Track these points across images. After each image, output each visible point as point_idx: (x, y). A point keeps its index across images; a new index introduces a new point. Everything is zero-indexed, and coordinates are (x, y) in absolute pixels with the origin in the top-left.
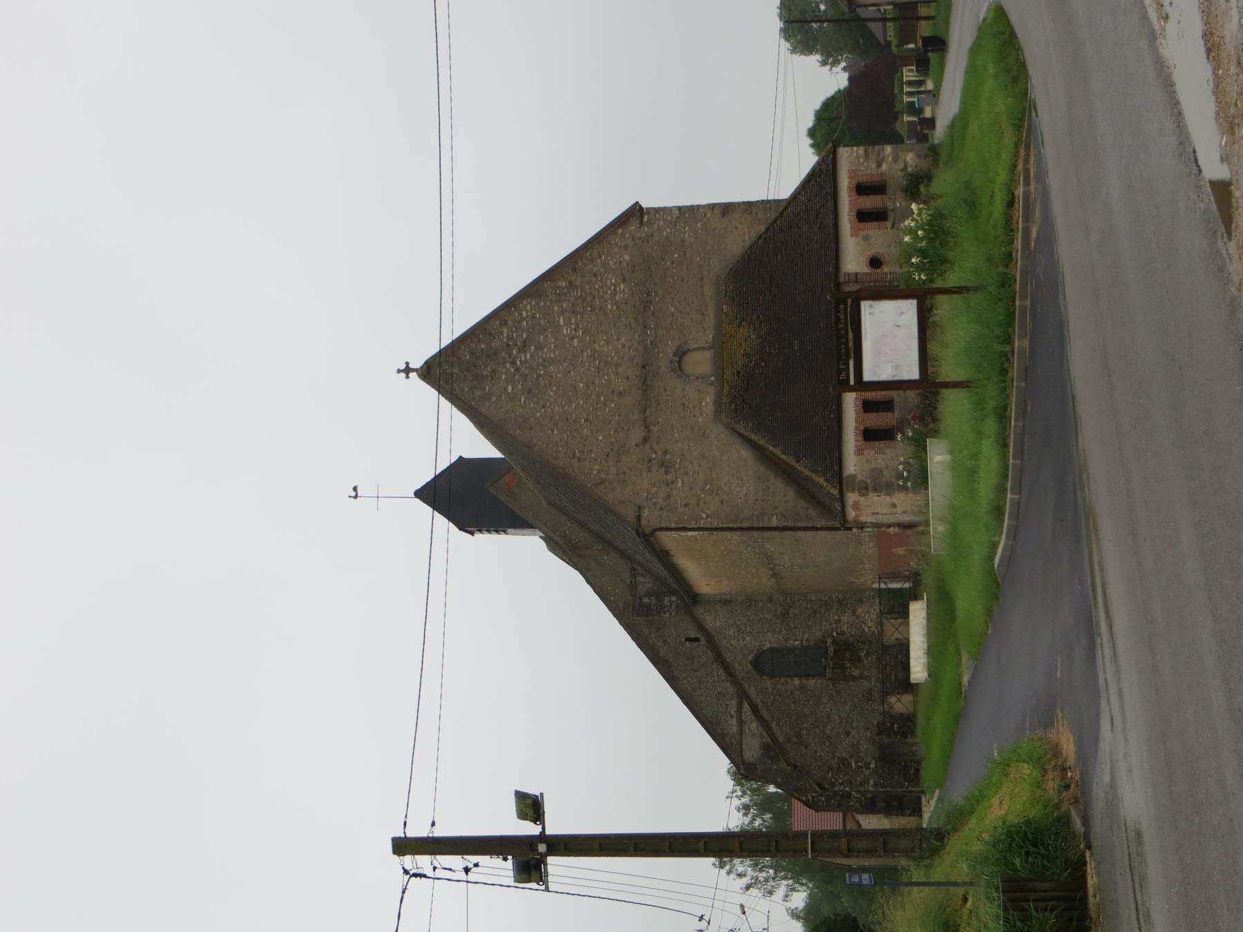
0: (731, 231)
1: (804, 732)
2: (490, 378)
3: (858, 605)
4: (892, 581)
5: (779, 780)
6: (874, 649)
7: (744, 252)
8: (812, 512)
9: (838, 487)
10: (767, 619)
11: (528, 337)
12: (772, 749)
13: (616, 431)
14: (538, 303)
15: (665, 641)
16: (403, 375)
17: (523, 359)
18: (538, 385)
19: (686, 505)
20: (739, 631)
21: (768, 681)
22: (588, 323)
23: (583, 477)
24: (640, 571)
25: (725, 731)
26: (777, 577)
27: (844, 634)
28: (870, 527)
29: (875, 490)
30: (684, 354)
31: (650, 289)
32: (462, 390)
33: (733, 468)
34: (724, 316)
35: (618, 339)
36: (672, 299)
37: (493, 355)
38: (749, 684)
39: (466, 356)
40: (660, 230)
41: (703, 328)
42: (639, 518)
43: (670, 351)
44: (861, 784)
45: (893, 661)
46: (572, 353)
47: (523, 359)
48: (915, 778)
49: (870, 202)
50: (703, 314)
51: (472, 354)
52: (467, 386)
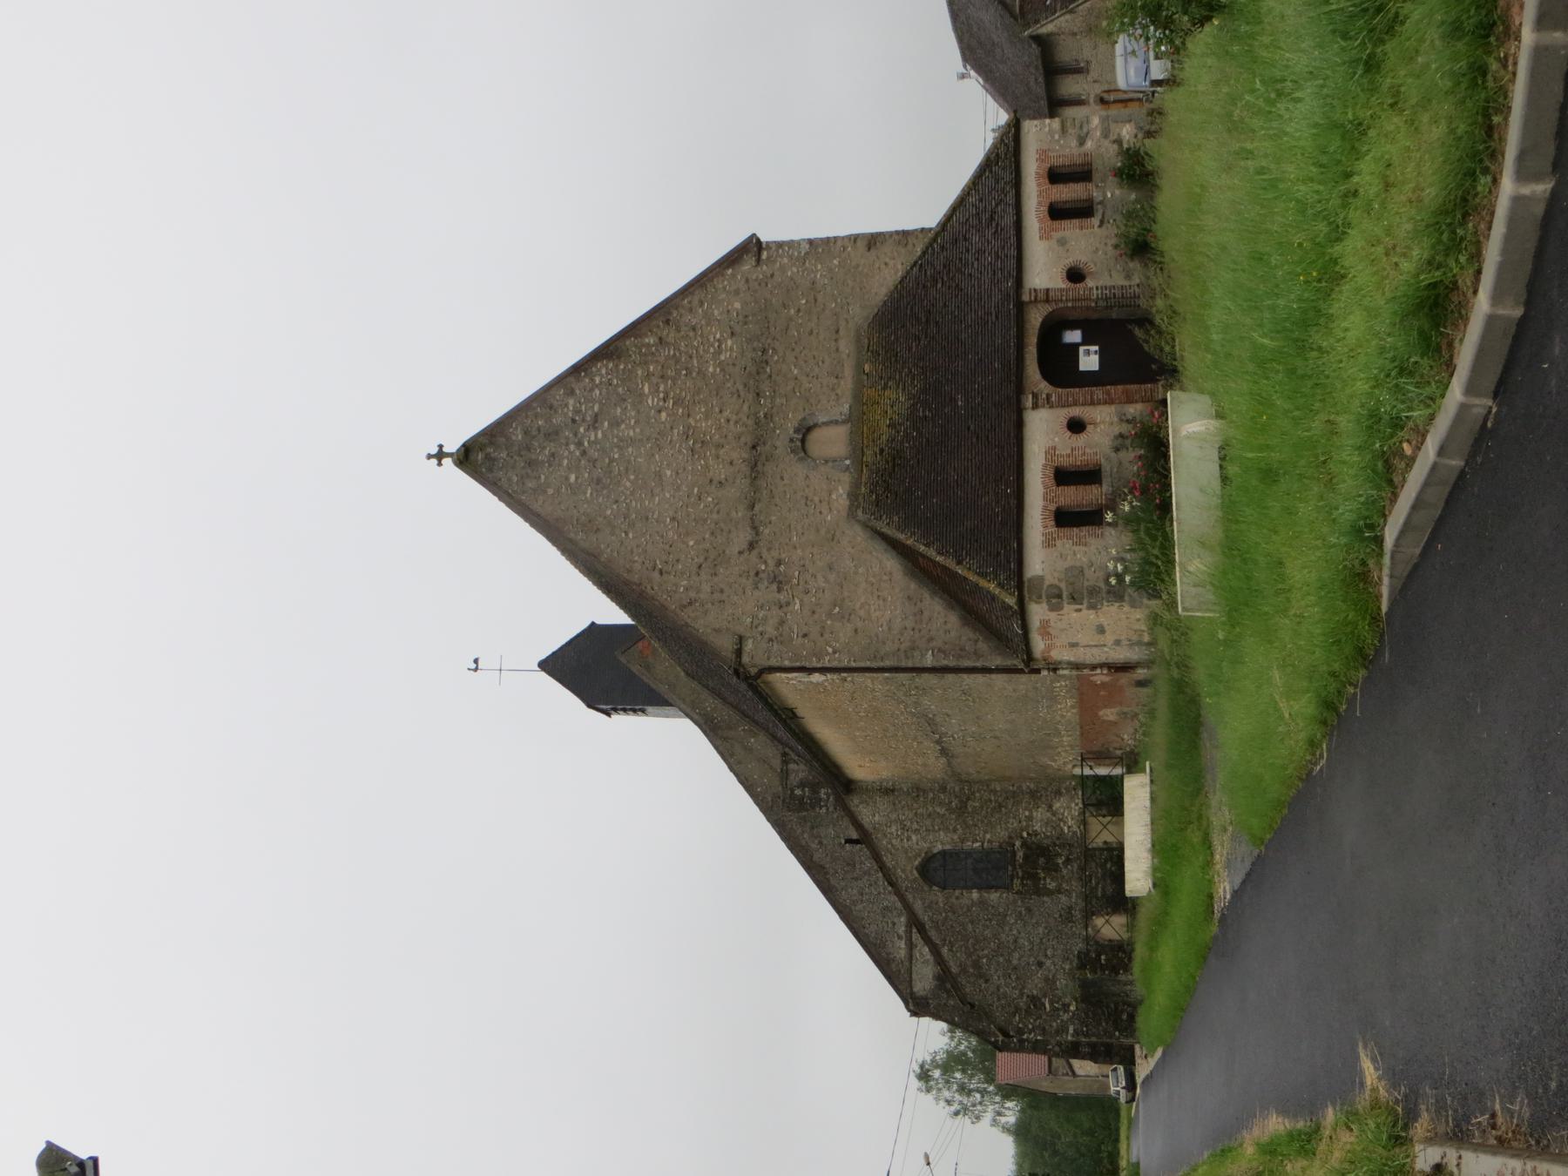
0: (879, 268)
1: (984, 960)
2: (547, 465)
3: (1055, 797)
4: (1100, 765)
5: (956, 1019)
6: (1075, 855)
7: (892, 288)
8: (983, 646)
9: (1016, 593)
10: (938, 813)
11: (601, 409)
12: (945, 977)
13: (712, 533)
14: (617, 366)
15: (820, 843)
16: (434, 461)
17: (593, 438)
18: (611, 472)
19: (805, 635)
20: (903, 829)
21: (939, 894)
22: (681, 390)
23: (665, 597)
24: (793, 755)
25: (892, 956)
26: (947, 755)
27: (1036, 835)
28: (1066, 669)
29: (1074, 599)
30: (809, 429)
31: (767, 346)
32: (509, 480)
33: (873, 584)
34: (865, 377)
35: (721, 412)
36: (796, 358)
37: (552, 435)
38: (914, 897)
39: (517, 436)
40: (783, 269)
41: (837, 395)
42: (739, 653)
43: (790, 426)
44: (1057, 1032)
45: (1100, 870)
46: (658, 430)
47: (593, 438)
48: (1129, 1027)
49: (1068, 193)
50: (837, 377)
51: (525, 433)
52: (517, 475)
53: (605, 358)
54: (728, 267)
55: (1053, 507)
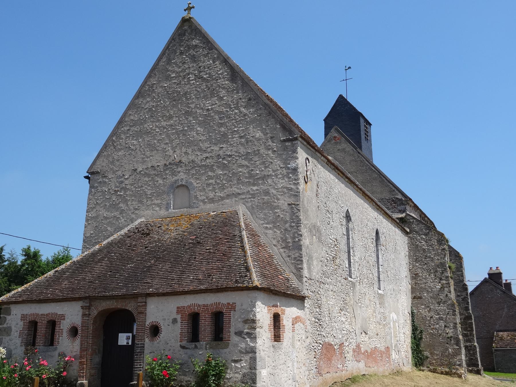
53: (232, 73)
54: (281, 125)
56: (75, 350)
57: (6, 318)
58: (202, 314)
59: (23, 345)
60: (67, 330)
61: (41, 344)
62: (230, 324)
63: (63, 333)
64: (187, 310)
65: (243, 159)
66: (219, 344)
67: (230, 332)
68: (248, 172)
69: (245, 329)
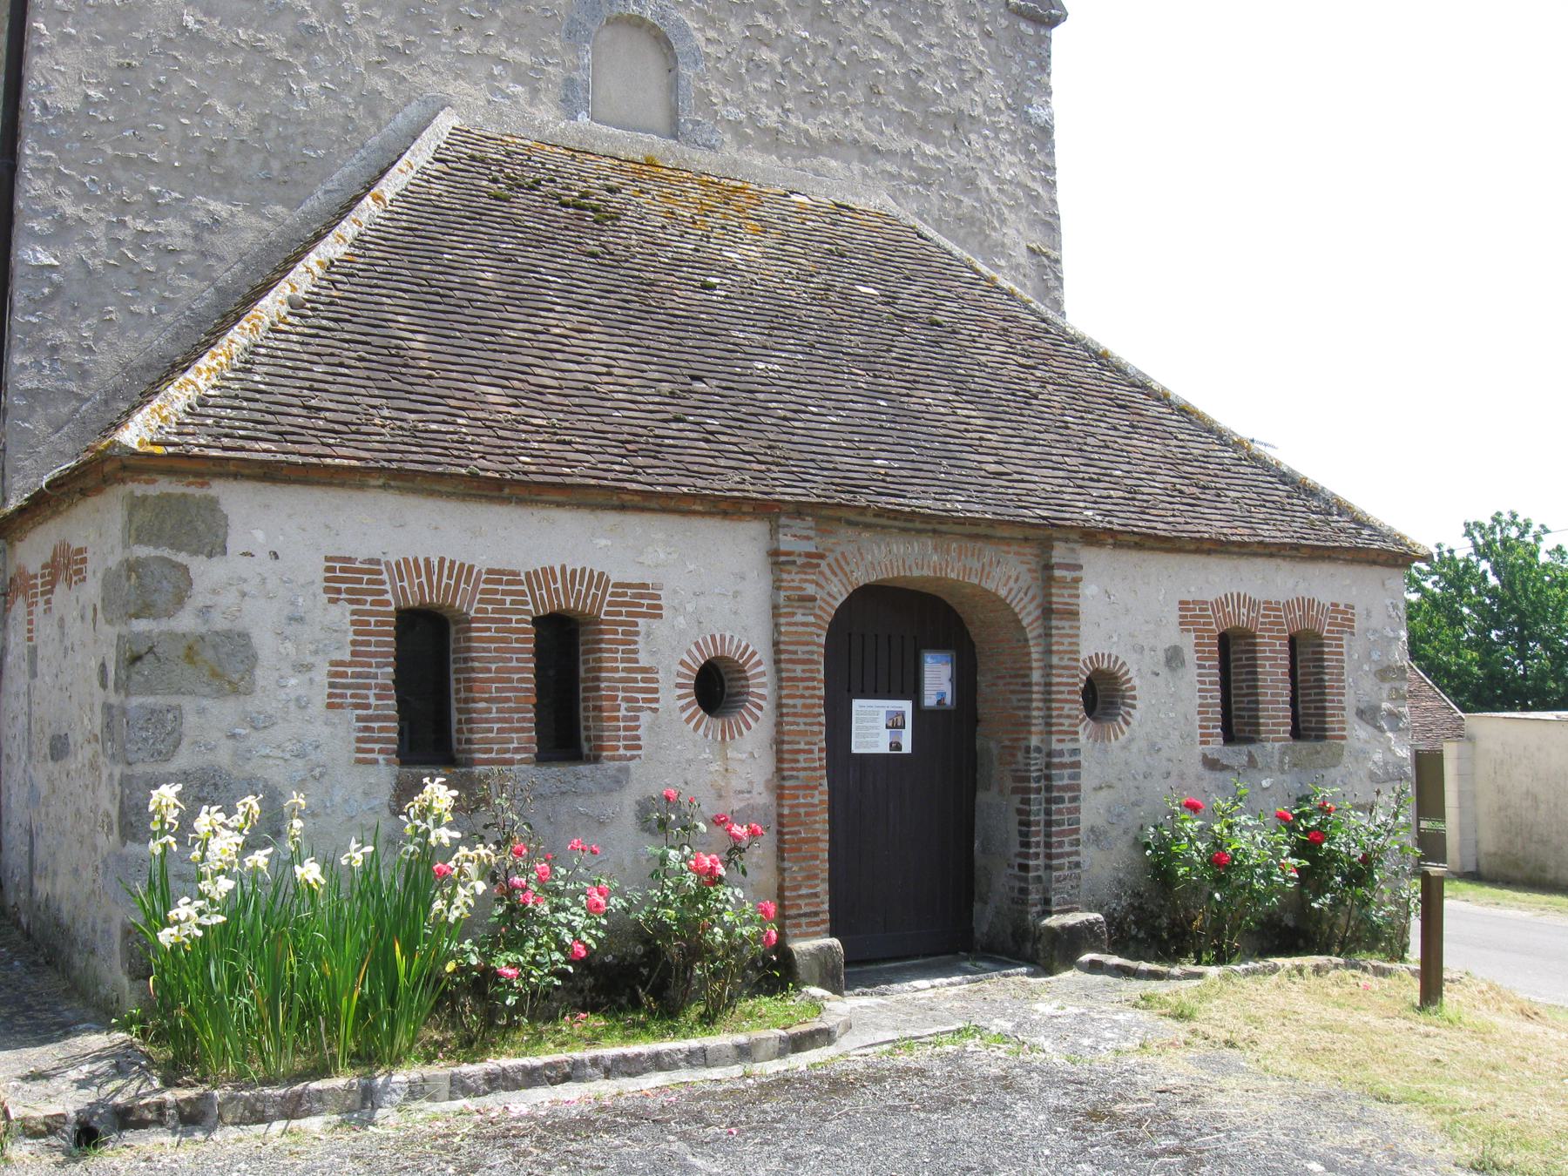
55: (467, 602)
56: (736, 783)
57: (186, 569)
58: (1264, 637)
59: (381, 758)
60: (679, 675)
61: (516, 750)
62: (1343, 681)
63: (656, 691)
64: (1286, 617)
65: (885, 16)
66: (1318, 753)
67: (1343, 709)
68: (906, 76)
69: (1382, 700)
